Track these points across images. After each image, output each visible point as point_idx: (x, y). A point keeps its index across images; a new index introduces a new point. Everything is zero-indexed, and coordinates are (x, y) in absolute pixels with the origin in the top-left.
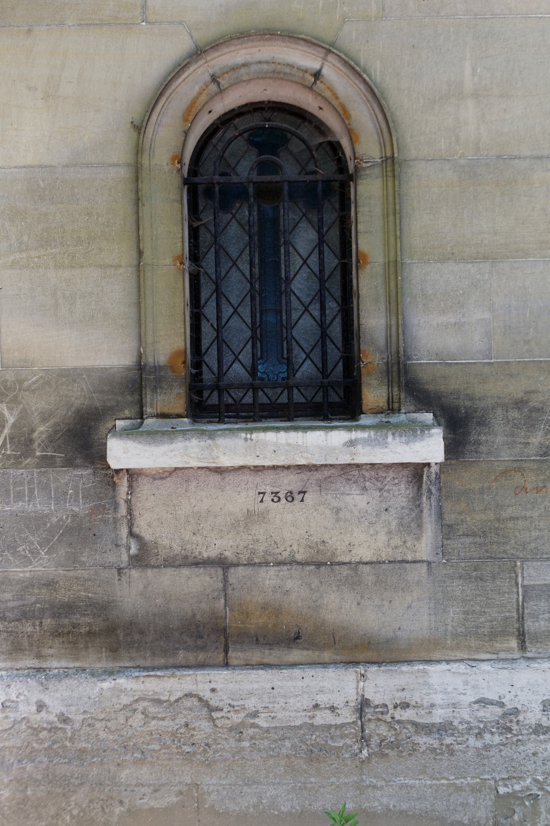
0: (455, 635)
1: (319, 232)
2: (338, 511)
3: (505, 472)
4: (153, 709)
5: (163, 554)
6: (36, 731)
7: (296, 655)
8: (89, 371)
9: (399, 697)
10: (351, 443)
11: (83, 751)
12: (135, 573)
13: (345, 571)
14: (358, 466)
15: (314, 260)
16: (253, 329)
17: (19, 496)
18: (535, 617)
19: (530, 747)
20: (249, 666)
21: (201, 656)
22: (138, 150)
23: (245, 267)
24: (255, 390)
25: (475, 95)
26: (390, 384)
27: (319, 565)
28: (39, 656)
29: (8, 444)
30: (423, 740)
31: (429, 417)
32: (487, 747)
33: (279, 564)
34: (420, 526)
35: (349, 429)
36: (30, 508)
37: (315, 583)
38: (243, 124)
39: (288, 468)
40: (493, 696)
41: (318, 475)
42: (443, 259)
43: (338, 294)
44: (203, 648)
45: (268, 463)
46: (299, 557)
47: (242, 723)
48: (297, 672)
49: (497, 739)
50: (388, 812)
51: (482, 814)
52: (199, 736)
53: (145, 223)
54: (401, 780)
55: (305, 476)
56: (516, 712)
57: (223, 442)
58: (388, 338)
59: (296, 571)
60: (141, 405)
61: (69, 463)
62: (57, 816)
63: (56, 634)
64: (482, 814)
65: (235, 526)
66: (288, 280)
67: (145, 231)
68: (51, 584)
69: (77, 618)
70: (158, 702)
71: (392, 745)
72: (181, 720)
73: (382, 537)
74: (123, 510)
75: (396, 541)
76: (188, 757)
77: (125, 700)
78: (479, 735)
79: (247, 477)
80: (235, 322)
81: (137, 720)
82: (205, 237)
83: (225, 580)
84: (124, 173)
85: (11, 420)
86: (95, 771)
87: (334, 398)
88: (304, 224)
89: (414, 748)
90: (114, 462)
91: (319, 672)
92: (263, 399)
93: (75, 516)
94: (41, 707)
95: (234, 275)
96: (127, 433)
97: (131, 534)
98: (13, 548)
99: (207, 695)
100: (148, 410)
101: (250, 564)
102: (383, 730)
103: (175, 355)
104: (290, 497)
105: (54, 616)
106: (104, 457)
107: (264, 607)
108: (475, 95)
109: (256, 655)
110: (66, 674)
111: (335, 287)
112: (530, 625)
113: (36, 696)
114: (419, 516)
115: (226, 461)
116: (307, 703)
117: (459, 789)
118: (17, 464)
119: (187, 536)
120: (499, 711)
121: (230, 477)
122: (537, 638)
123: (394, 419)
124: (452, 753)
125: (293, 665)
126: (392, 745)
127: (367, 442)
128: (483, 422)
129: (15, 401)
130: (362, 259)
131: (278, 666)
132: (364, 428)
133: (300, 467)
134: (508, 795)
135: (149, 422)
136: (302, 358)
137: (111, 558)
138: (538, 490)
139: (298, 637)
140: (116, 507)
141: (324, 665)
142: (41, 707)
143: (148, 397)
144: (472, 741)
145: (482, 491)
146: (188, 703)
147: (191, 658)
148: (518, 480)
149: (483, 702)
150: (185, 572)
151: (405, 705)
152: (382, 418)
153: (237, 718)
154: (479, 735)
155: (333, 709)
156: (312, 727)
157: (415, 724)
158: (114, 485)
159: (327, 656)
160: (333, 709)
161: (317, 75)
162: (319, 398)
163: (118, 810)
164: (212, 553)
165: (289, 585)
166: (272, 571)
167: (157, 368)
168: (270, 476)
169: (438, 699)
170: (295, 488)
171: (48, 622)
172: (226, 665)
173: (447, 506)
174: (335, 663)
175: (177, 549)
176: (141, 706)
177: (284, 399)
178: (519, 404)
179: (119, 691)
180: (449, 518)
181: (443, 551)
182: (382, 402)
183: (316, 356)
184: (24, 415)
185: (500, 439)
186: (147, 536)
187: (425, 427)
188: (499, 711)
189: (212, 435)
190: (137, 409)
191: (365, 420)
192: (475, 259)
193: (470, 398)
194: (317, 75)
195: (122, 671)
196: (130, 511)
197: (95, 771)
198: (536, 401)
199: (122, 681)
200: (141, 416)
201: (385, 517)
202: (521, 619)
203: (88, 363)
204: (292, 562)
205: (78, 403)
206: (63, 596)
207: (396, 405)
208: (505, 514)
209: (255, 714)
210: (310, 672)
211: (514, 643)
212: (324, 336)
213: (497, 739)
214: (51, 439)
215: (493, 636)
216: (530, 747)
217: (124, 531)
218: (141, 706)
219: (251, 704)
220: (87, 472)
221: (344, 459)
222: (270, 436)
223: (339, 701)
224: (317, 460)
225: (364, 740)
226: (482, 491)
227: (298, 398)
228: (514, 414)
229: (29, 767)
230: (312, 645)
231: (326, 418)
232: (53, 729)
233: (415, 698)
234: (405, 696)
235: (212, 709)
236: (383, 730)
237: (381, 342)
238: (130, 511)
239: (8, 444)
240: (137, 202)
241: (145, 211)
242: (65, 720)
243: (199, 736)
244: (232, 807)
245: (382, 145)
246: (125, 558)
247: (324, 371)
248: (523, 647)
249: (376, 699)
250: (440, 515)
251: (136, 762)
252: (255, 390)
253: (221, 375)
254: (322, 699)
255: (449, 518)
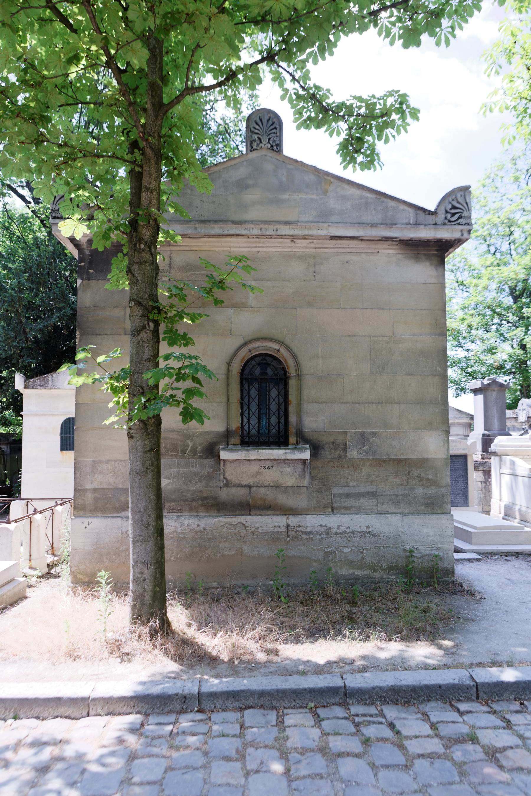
0: (314, 507)
1: (278, 391)
2: (282, 472)
3: (328, 462)
4: (229, 527)
5: (233, 483)
6: (196, 532)
7: (269, 512)
8: (213, 432)
9: (298, 524)
10: (286, 453)
11: (210, 538)
12: (225, 489)
13: (284, 489)
14: (288, 459)
15: (276, 400)
16: (258, 406)
17: (193, 467)
18: (336, 502)
19: (334, 538)
20: (256, 515)
21: (243, 512)
22: (228, 371)
23: (257, 401)
25: (322, 357)
26: (297, 437)
27: (276, 487)
28: (197, 512)
29: (426, 491)
30: (305, 536)
31: (308, 446)
32: (322, 538)
33: (265, 487)
35: (285, 449)
36: (196, 470)
37: (275, 492)
38: (258, 360)
39: (268, 460)
41: (276, 462)
42: (312, 402)
43: (283, 410)
44: (243, 510)
45: (263, 458)
47: (254, 531)
48: (270, 517)
49: (325, 536)
50: (294, 556)
51: (320, 557)
52: (242, 534)
53: (230, 391)
54: (298, 547)
55: (273, 462)
56: (330, 528)
57: (252, 452)
58: (297, 424)
59: (270, 489)
60: (228, 442)
61: (207, 457)
62: (202, 557)
63: (202, 505)
64: (320, 557)
65: (253, 476)
67: (230, 393)
68: (201, 491)
69: (208, 501)
70: (231, 524)
71: (296, 537)
72: (237, 530)
73: (294, 480)
74: (222, 471)
75: (298, 481)
76: (239, 540)
77: (222, 524)
78: (320, 535)
79: (257, 462)
80: (253, 417)
81: (225, 530)
82: (245, 392)
83: (250, 491)
84: (224, 376)
85: (191, 445)
86: (213, 544)
87: (282, 440)
88: (274, 389)
89: (302, 538)
90: (221, 458)
91: (276, 517)
94: (198, 525)
95: (253, 403)
96: (224, 449)
97: (224, 478)
98: (191, 481)
99: (245, 523)
100: (230, 443)
101: (257, 487)
102: (293, 533)
103: (237, 428)
104: (269, 468)
105: (202, 500)
106: (219, 456)
107: (261, 499)
108: (322, 357)
109: (258, 512)
110: (205, 517)
111: (282, 407)
112: (335, 505)
113: (197, 523)
114: (305, 474)
115: (252, 457)
116: (272, 525)
117: (314, 550)
118: (192, 457)
119: (240, 478)
120: (325, 528)
121: (252, 462)
122: (337, 508)
123: (298, 447)
124: (312, 540)
125: (269, 515)
126: (296, 537)
128: (323, 448)
129: (192, 440)
130: (290, 402)
131: (265, 515)
132: (289, 449)
133: (271, 460)
134: (327, 552)
135: (230, 446)
137: (218, 484)
138: (338, 467)
139: (270, 507)
140: (220, 470)
141: (277, 515)
142: (198, 525)
143: (230, 440)
144: (318, 537)
145: (322, 467)
146: (239, 525)
147: (240, 513)
148: (332, 464)
150: (239, 488)
151: (300, 526)
152: (294, 446)
153: (253, 529)
154: (320, 535)
155: (279, 527)
156: (274, 532)
157: (302, 532)
158: (219, 464)
159: (278, 513)
160: (279, 527)
161: (278, 350)
162: (277, 440)
163: (219, 555)
164: (246, 483)
165: (268, 492)
166: (263, 489)
167: (232, 431)
168: (263, 462)
169: (309, 525)
170: (270, 465)
171: (200, 502)
172: (250, 515)
173: (312, 471)
174: (280, 515)
175: (237, 482)
176: (226, 526)
177: (267, 440)
178: (333, 443)
180: (313, 474)
181: (311, 484)
184: (194, 444)
185: (327, 453)
186: (228, 478)
187: (306, 449)
188: (325, 528)
189: (248, 450)
190: (226, 443)
191: (290, 447)
192: (321, 402)
193: (319, 441)
194: (278, 350)
195: (221, 516)
196: (224, 471)
197: (213, 544)
198: (337, 442)
199: (221, 519)
200: (228, 444)
201: (295, 474)
202: (332, 503)
203: (213, 429)
204: (269, 486)
205: (210, 441)
206: (204, 495)
208: (328, 474)
209: (258, 528)
210: (273, 517)
211: (330, 510)
212: (279, 422)
213: (325, 536)
214: (202, 451)
215: (325, 508)
216: (334, 538)
217: (222, 477)
218: (226, 526)
219: (257, 525)
220: (212, 460)
221: (284, 457)
222: (264, 451)
223: (281, 525)
224: (277, 458)
225: (288, 536)
226: (322, 467)
227: (271, 440)
229: (194, 543)
230: (274, 509)
231: (279, 446)
232: (201, 532)
233: (302, 524)
234: (300, 524)
235: (246, 527)
236: (293, 533)
237: (295, 425)
238: (224, 471)
239: (426, 491)
240: (228, 385)
241: (230, 388)
242: (205, 529)
243: (242, 534)
244: (251, 554)
245: (296, 371)
248: (333, 511)
249: (292, 524)
250: (310, 474)
251: (224, 541)
253: (249, 433)
254: (276, 524)
255: (313, 474)
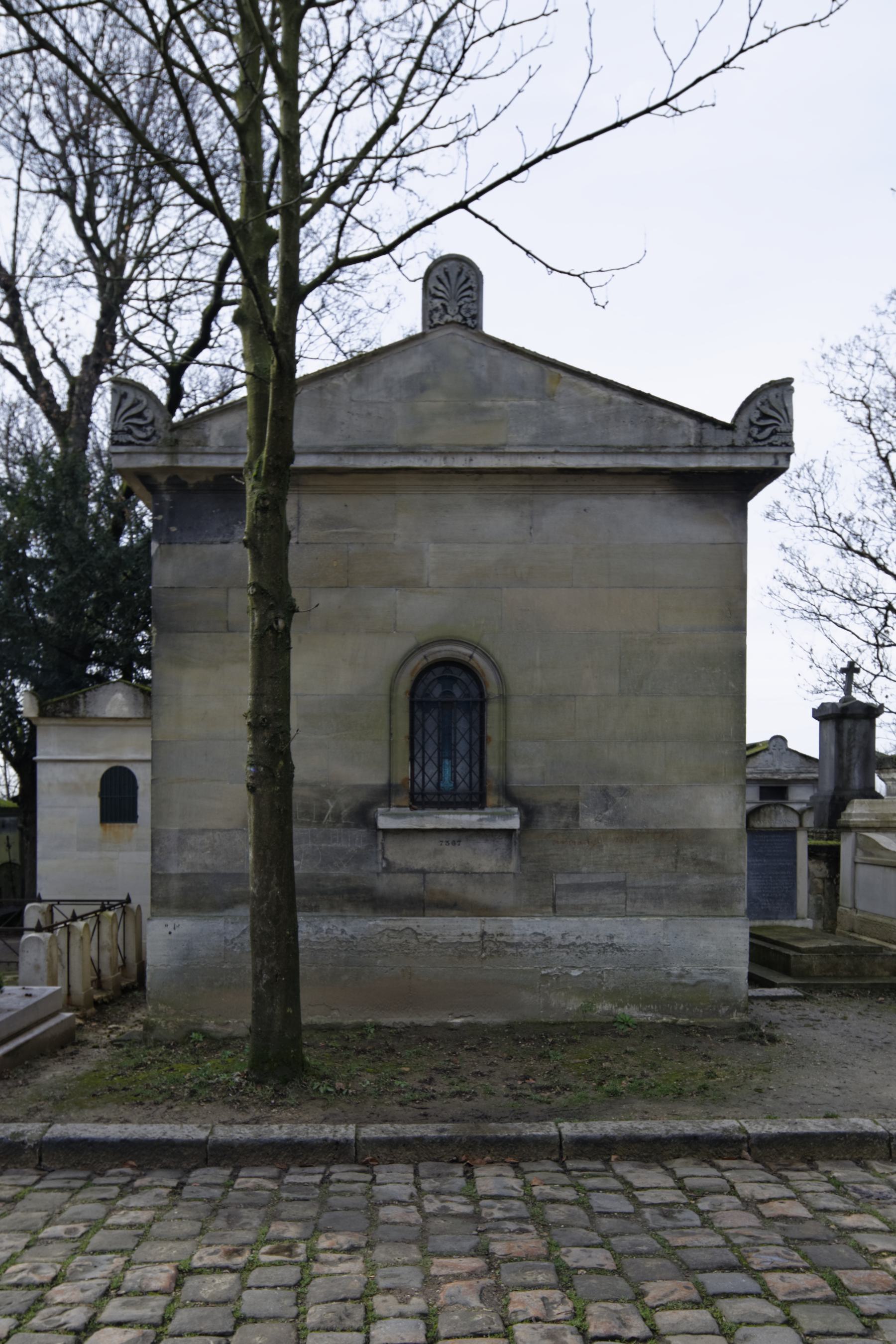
4: (392, 934)
6: (340, 942)
9: (500, 931)
10: (481, 820)
12: (384, 875)
13: (477, 876)
15: (467, 736)
17: (334, 841)
19: (556, 954)
24: (439, 795)
27: (466, 873)
28: (342, 911)
30: (509, 950)
31: (515, 809)
32: (537, 954)
33: (448, 872)
34: (511, 857)
40: (540, 931)
46: (457, 870)
52: (411, 946)
56: (550, 938)
66: (455, 745)
68: (347, 879)
70: (394, 931)
73: (494, 862)
74: (380, 848)
77: (380, 930)
78: (534, 948)
83: (424, 880)
85: (332, 807)
87: (474, 799)
92: (442, 800)
93: (358, 849)
97: (384, 858)
99: (415, 928)
101: (436, 872)
102: (492, 945)
106: (376, 824)
112: (558, 902)
116: (459, 932)
127: (487, 820)
130: (489, 739)
136: (233, 290)
140: (377, 846)
142: (343, 931)
144: (531, 951)
146: (407, 932)
149: (536, 934)
151: (501, 935)
153: (428, 938)
154: (534, 948)
156: (461, 943)
164: (418, 867)
166: (445, 876)
169: (516, 932)
171: (346, 896)
177: (451, 800)
178: (556, 804)
179: (377, 926)
182: (495, 803)
183: (467, 780)
191: (487, 810)
196: (383, 848)
202: (554, 899)
204: (453, 872)
207: (286, 1244)
209: (436, 937)
211: (551, 909)
213: (542, 950)
215: (542, 906)
216: (556, 954)
217: (380, 857)
219: (435, 932)
220: (364, 830)
221: (477, 826)
222: (447, 817)
223: (472, 932)
227: (458, 799)
228: (554, 809)
232: (348, 942)
233: (507, 931)
240: (391, 712)
246: (380, 869)
247: (471, 787)
248: (555, 911)
252: (439, 795)
254: (466, 931)
